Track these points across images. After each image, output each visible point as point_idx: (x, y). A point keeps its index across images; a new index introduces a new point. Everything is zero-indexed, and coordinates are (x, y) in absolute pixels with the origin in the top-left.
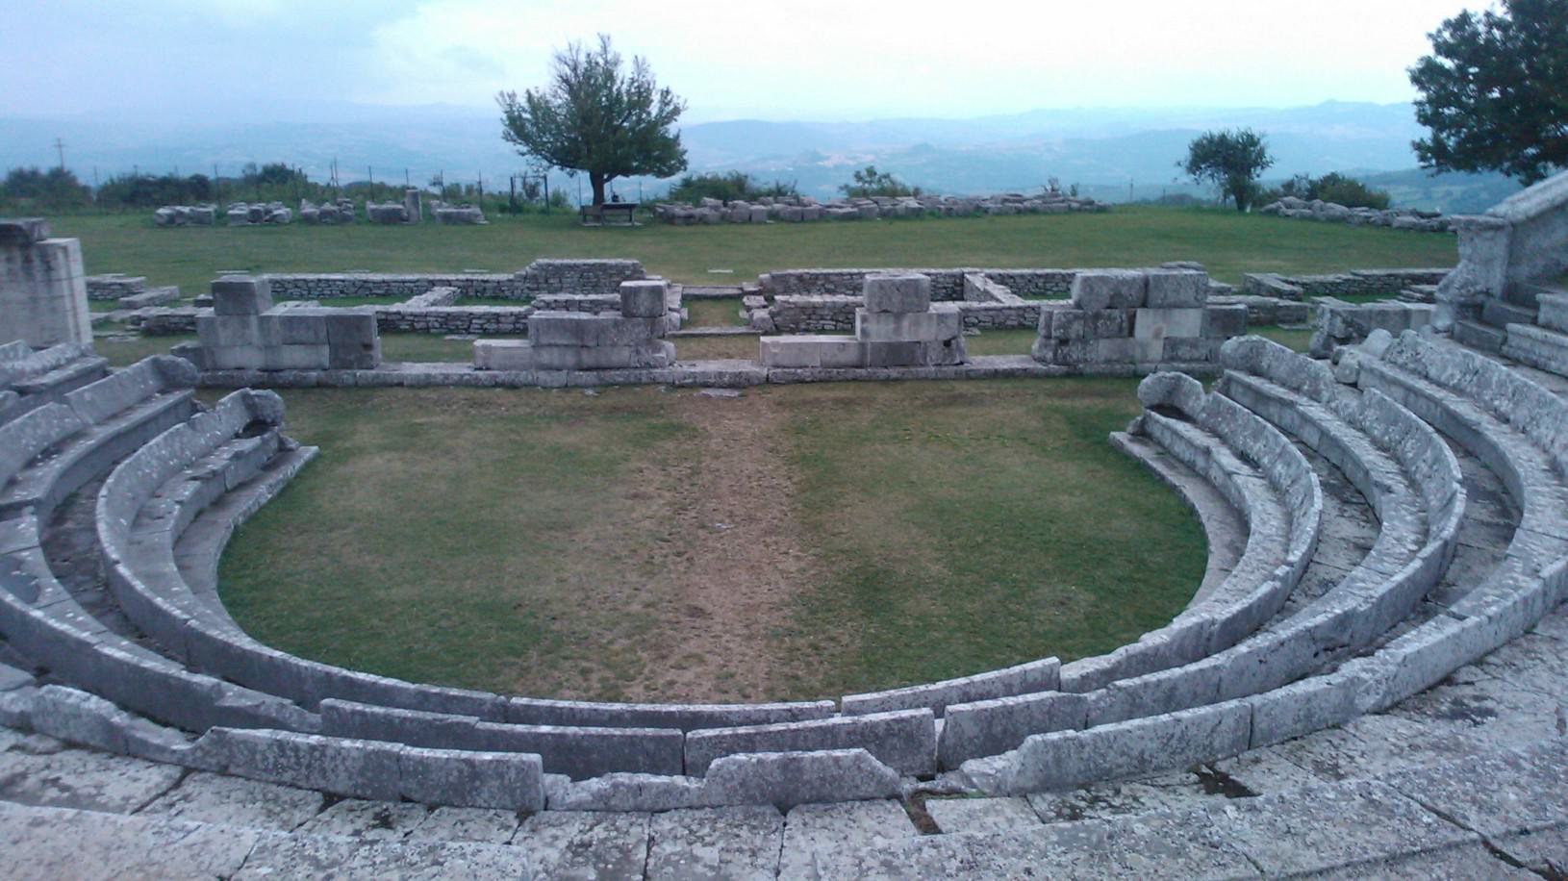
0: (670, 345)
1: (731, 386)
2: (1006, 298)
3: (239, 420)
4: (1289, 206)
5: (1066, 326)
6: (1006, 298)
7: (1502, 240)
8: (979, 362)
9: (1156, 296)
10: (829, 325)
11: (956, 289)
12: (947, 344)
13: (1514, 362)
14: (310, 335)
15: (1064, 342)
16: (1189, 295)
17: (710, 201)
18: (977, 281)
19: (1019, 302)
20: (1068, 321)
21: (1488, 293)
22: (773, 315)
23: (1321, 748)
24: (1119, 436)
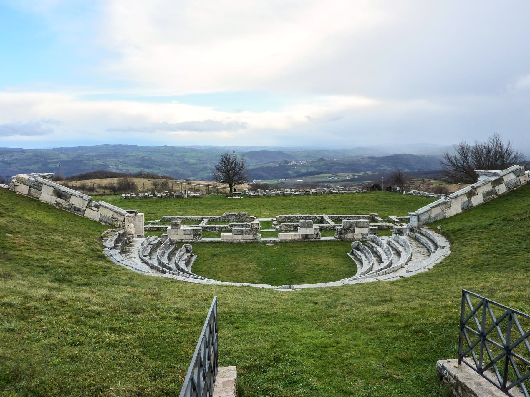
0: (260, 235)
1: (273, 243)
2: (331, 223)
3: (184, 250)
4: (414, 192)
5: (341, 231)
6: (331, 223)
7: (416, 217)
8: (323, 238)
9: (359, 225)
10: (293, 229)
11: (322, 221)
12: (317, 234)
13: (20, 293)
14: (189, 233)
15: (341, 234)
16: (366, 224)
17: (260, 190)
18: (326, 218)
19: (334, 224)
20: (342, 230)
21: (415, 227)
22: (280, 227)
23: (500, 365)
24: (348, 253)
